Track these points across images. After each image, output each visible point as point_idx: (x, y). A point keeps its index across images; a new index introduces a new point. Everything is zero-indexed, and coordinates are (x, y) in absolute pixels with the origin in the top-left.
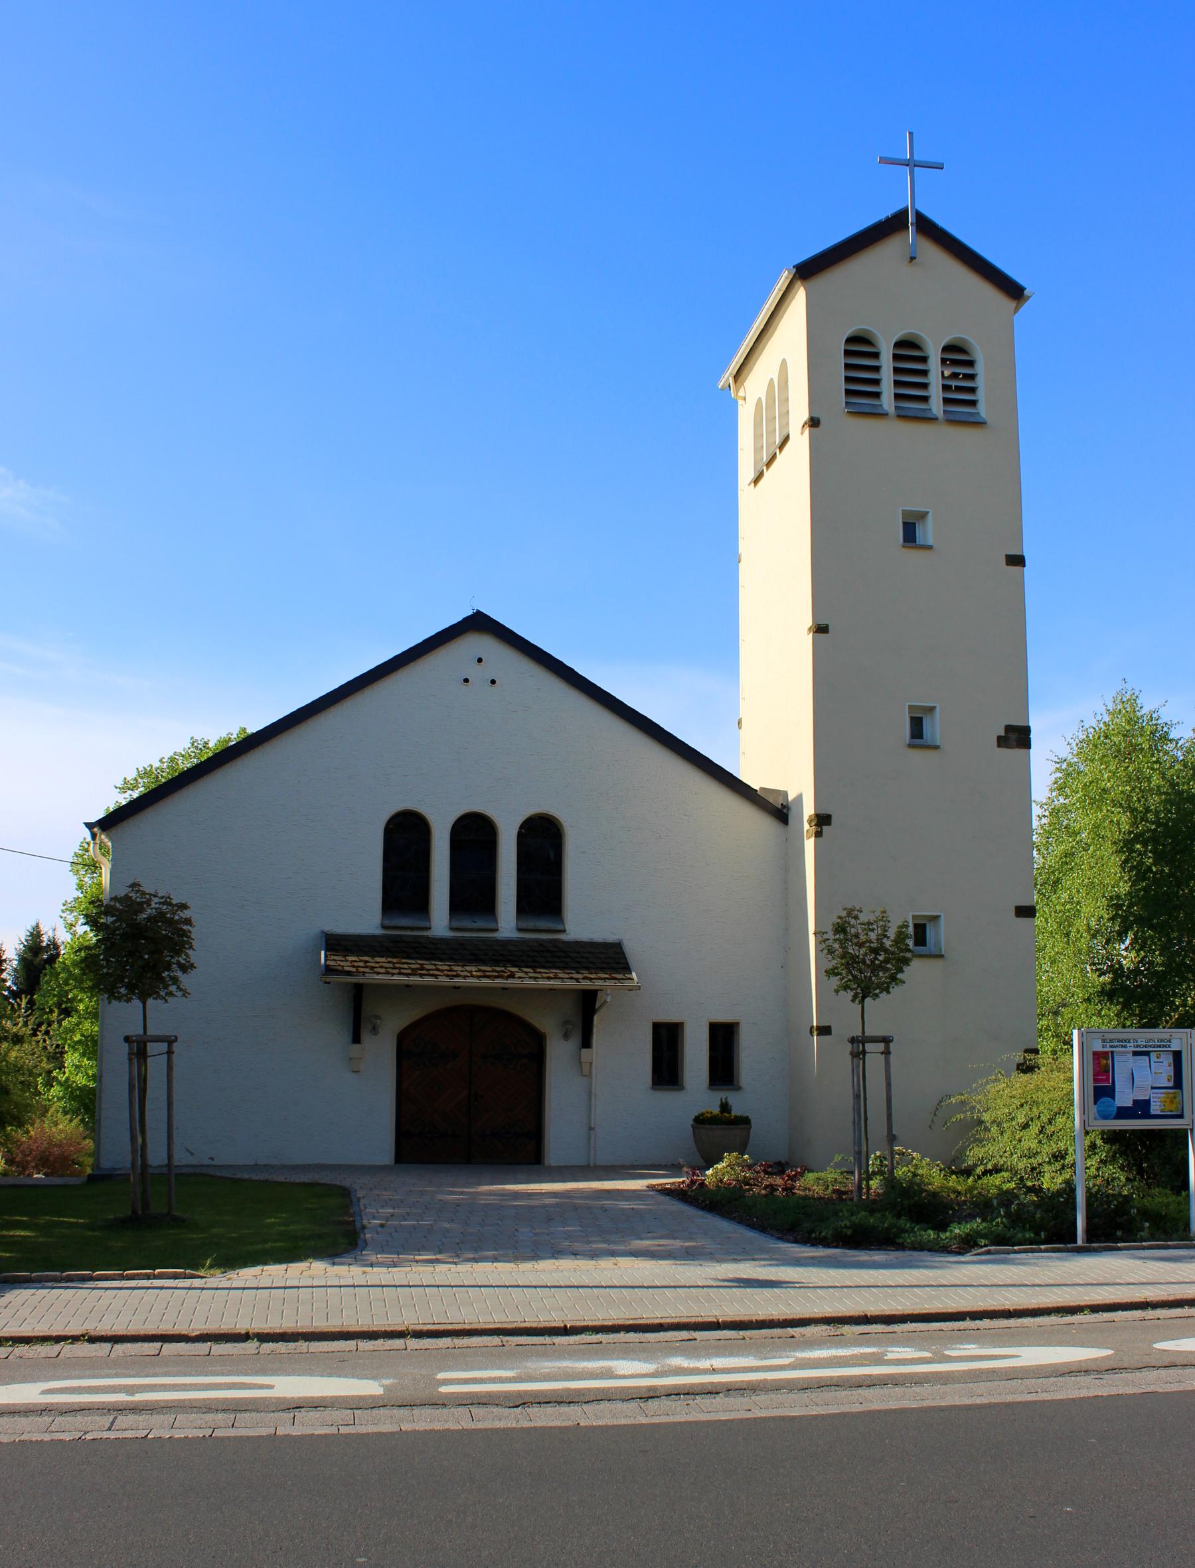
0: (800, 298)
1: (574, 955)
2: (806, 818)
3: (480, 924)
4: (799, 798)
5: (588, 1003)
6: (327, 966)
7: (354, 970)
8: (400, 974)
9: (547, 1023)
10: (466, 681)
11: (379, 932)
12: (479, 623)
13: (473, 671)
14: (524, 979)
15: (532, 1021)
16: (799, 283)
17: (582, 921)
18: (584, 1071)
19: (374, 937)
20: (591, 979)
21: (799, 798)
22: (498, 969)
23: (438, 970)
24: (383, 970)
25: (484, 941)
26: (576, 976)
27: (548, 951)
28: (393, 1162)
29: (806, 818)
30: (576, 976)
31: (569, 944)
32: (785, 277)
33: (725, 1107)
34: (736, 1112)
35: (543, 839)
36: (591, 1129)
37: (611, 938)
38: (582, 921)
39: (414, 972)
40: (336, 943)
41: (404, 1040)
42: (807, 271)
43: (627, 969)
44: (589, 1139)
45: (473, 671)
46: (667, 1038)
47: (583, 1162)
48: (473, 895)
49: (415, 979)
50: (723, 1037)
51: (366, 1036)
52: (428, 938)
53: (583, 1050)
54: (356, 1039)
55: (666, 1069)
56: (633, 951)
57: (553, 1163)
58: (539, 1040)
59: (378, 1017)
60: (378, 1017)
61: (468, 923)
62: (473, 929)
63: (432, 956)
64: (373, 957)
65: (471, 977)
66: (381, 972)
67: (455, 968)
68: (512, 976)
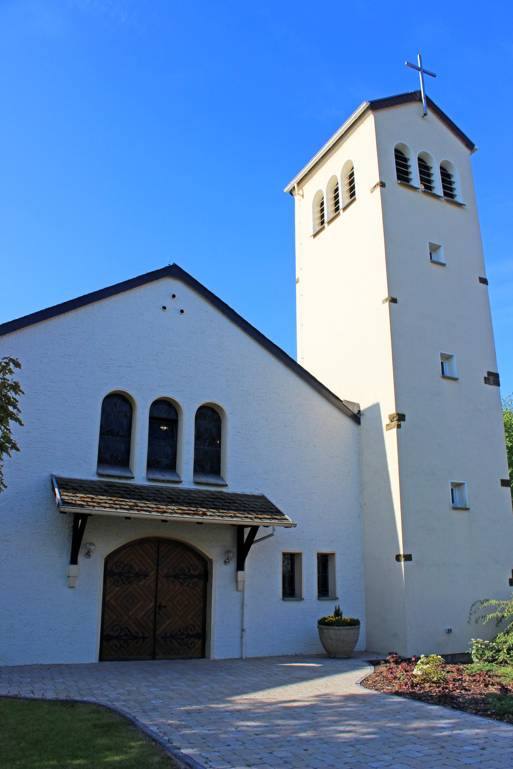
0: (370, 120)
2: (385, 420)
3: (168, 477)
4: (376, 408)
6: (62, 500)
7: (85, 503)
8: (122, 508)
9: (215, 551)
10: (164, 308)
11: (96, 478)
12: (174, 272)
13: (169, 303)
15: (201, 549)
16: (370, 112)
17: (237, 477)
20: (261, 519)
21: (376, 408)
24: (107, 505)
25: (173, 489)
28: (94, 657)
29: (385, 420)
32: (364, 105)
33: (338, 613)
34: (346, 616)
35: (210, 419)
38: (237, 477)
39: (131, 508)
40: (65, 484)
41: (108, 560)
42: (375, 106)
44: (242, 637)
45: (169, 303)
46: (291, 561)
48: (162, 458)
50: (324, 561)
51: (81, 558)
52: (132, 485)
54: (74, 561)
55: (290, 588)
57: (217, 657)
60: (92, 544)
61: (159, 476)
62: (162, 481)
63: (141, 498)
64: (97, 495)
66: (103, 507)
68: (204, 514)
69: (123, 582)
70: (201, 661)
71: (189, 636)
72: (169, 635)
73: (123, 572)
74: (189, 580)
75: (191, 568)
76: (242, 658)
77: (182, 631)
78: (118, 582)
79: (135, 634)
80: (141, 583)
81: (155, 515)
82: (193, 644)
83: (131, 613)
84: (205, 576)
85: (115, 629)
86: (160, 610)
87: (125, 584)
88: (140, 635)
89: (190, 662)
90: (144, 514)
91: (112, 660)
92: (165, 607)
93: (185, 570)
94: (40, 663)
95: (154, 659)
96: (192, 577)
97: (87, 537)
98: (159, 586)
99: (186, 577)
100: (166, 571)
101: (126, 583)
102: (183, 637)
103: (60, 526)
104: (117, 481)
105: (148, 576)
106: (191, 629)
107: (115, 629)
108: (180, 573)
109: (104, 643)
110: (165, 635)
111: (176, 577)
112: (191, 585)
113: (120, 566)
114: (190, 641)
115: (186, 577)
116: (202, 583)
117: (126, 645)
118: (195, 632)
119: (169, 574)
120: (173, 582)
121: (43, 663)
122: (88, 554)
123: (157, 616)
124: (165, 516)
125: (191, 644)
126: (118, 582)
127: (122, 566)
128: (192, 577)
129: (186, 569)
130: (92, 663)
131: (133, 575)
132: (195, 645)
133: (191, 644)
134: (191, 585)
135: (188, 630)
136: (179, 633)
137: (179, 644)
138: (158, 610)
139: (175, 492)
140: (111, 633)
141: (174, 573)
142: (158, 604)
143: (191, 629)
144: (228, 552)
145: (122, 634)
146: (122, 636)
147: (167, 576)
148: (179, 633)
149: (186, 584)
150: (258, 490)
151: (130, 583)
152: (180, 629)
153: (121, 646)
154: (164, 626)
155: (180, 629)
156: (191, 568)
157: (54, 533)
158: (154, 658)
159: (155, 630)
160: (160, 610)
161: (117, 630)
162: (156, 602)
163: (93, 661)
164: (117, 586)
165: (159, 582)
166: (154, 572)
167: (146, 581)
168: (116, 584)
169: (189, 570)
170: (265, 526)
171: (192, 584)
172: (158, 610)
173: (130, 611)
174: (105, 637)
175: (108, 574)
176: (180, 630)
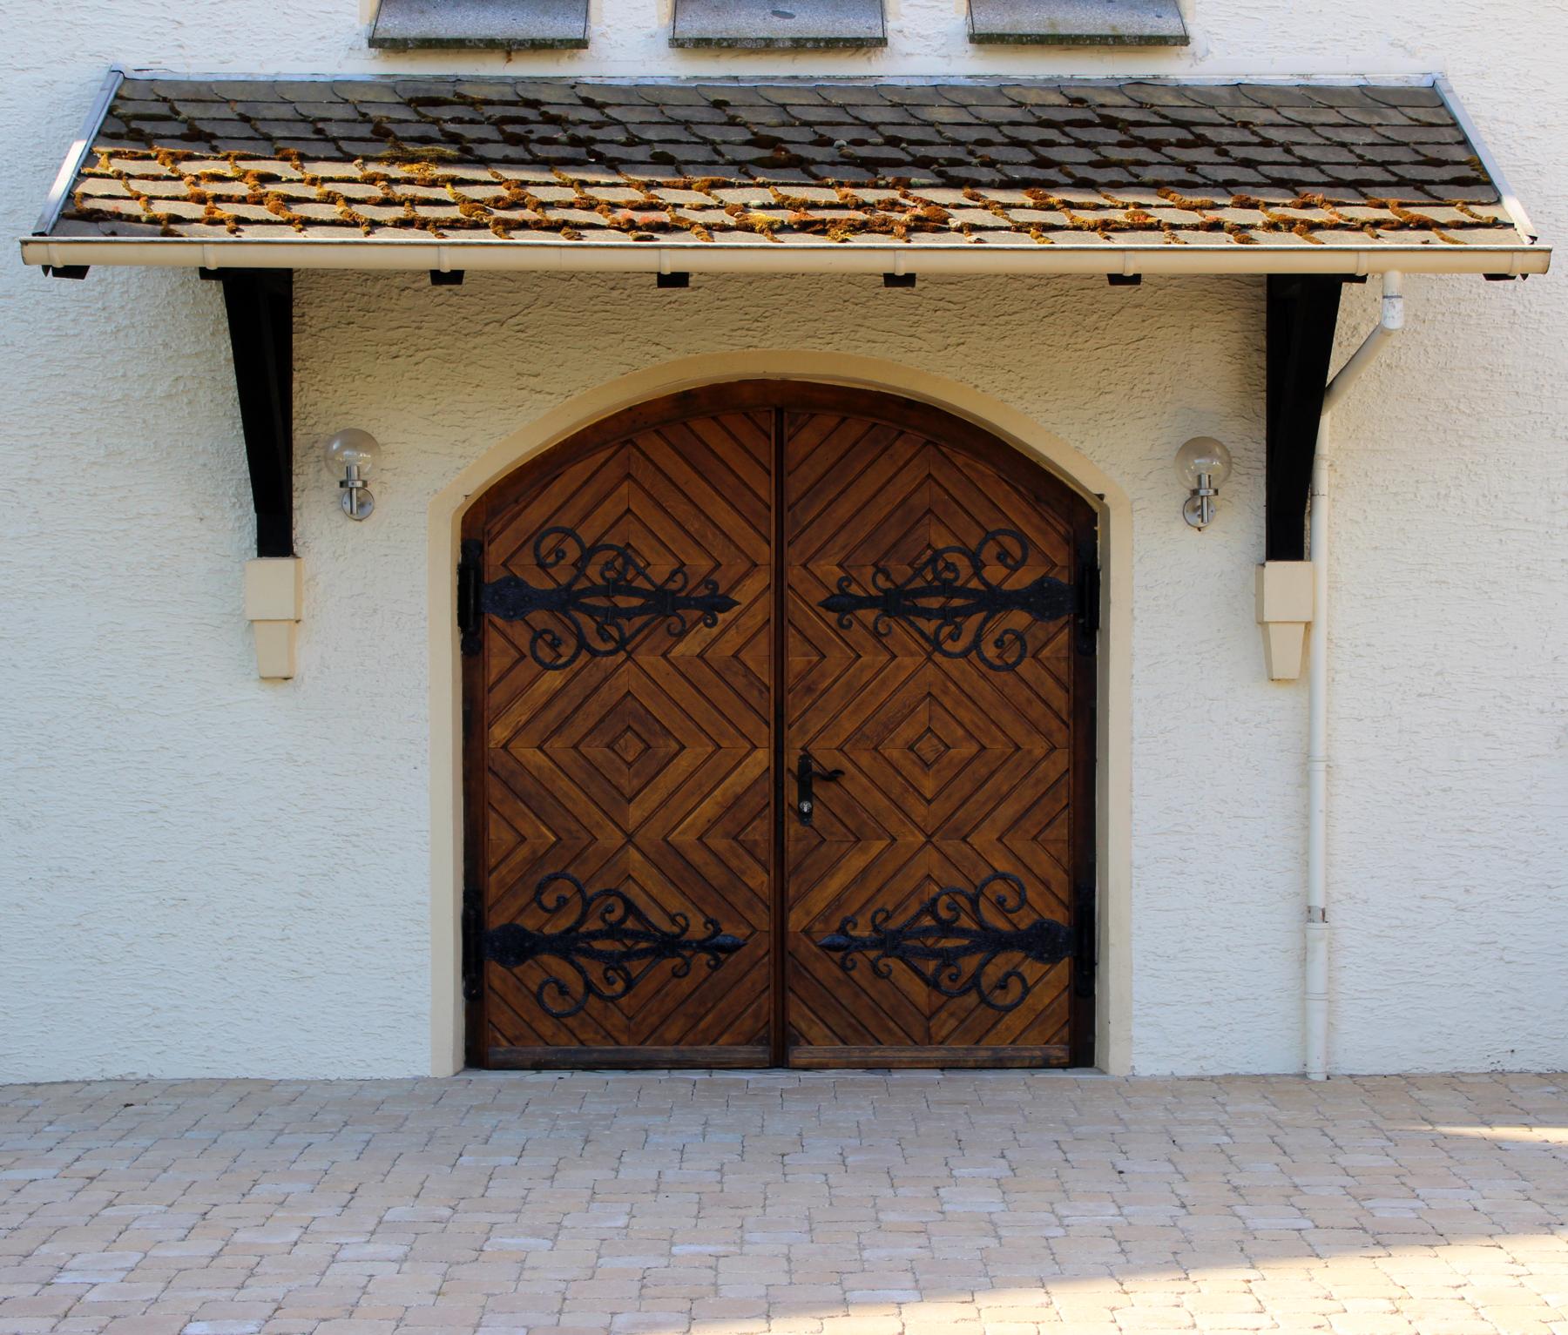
1: (1227, 135)
5: (1296, 334)
9: (1132, 441)
11: (366, 66)
14: (988, 239)
18: (1282, 662)
19: (336, 90)
22: (869, 195)
23: (590, 206)
26: (1233, 216)
27: (1110, 123)
30: (1233, 216)
31: (1202, 97)
36: (1313, 915)
37: (1393, 68)
43: (1475, 179)
44: (1304, 959)
47: (1275, 1059)
49: (471, 251)
51: (313, 515)
52: (880, 92)
53: (1277, 569)
54: (275, 536)
56: (1493, 124)
58: (1077, 520)
59: (361, 439)
60: (361, 439)
65: (738, 236)
67: (668, 196)
68: (933, 222)
69: (583, 645)
70: (1065, 1086)
71: (993, 942)
72: (863, 931)
73: (582, 584)
74: (978, 618)
75: (990, 552)
76: (1304, 1076)
77: (944, 914)
78: (554, 645)
79: (666, 926)
80: (687, 647)
81: (608, 250)
82: (1015, 988)
83: (635, 813)
84: (1076, 600)
85: (549, 900)
86: (806, 794)
87: (594, 653)
88: (698, 930)
89: (1012, 1085)
90: (535, 251)
91: (538, 1066)
92: (834, 776)
93: (950, 567)
94: (142, 1075)
95: (779, 1061)
96: (994, 601)
97: (316, 403)
98: (796, 661)
99: (957, 602)
100: (829, 569)
101: (600, 646)
102: (949, 943)
103: (187, 350)
104: (492, 67)
105: (727, 604)
106: (1000, 903)
107: (549, 900)
108: (918, 583)
109: (496, 973)
110: (842, 930)
111: (895, 603)
112: (990, 652)
113: (560, 555)
114: (994, 972)
115: (957, 602)
116: (1063, 637)
117: (619, 986)
118: (1025, 921)
119: (854, 589)
120: (877, 635)
121: (157, 1074)
122: (356, 497)
123: (793, 828)
124: (671, 253)
125: (1002, 985)
126: (554, 645)
127: (573, 552)
128: (994, 601)
129: (952, 557)
130: (417, 1080)
131: (636, 602)
132: (1027, 990)
133: (1002, 985)
134: (990, 652)
135: (983, 905)
136: (927, 921)
137: (932, 983)
138: (792, 792)
139: (828, 105)
140: (529, 923)
141: (881, 580)
142: (792, 761)
143: (1000, 903)
144: (1197, 446)
145: (593, 925)
146: (593, 935)
147: (841, 604)
148: (927, 921)
149: (958, 646)
150: (1412, 54)
151: (622, 644)
152: (934, 901)
153: (589, 988)
154: (835, 884)
155: (934, 901)
156: (990, 552)
157: (161, 389)
158: (779, 1051)
159: (780, 907)
160: (806, 794)
161: (562, 902)
162: (779, 752)
163: (425, 1069)
164: (548, 667)
165: (793, 640)
166: (759, 581)
167: (715, 630)
168: (545, 653)
169: (978, 567)
170: (1490, 277)
171: (999, 643)
172: (792, 792)
173: (630, 801)
174: (489, 945)
175: (479, 599)
176: (930, 908)
